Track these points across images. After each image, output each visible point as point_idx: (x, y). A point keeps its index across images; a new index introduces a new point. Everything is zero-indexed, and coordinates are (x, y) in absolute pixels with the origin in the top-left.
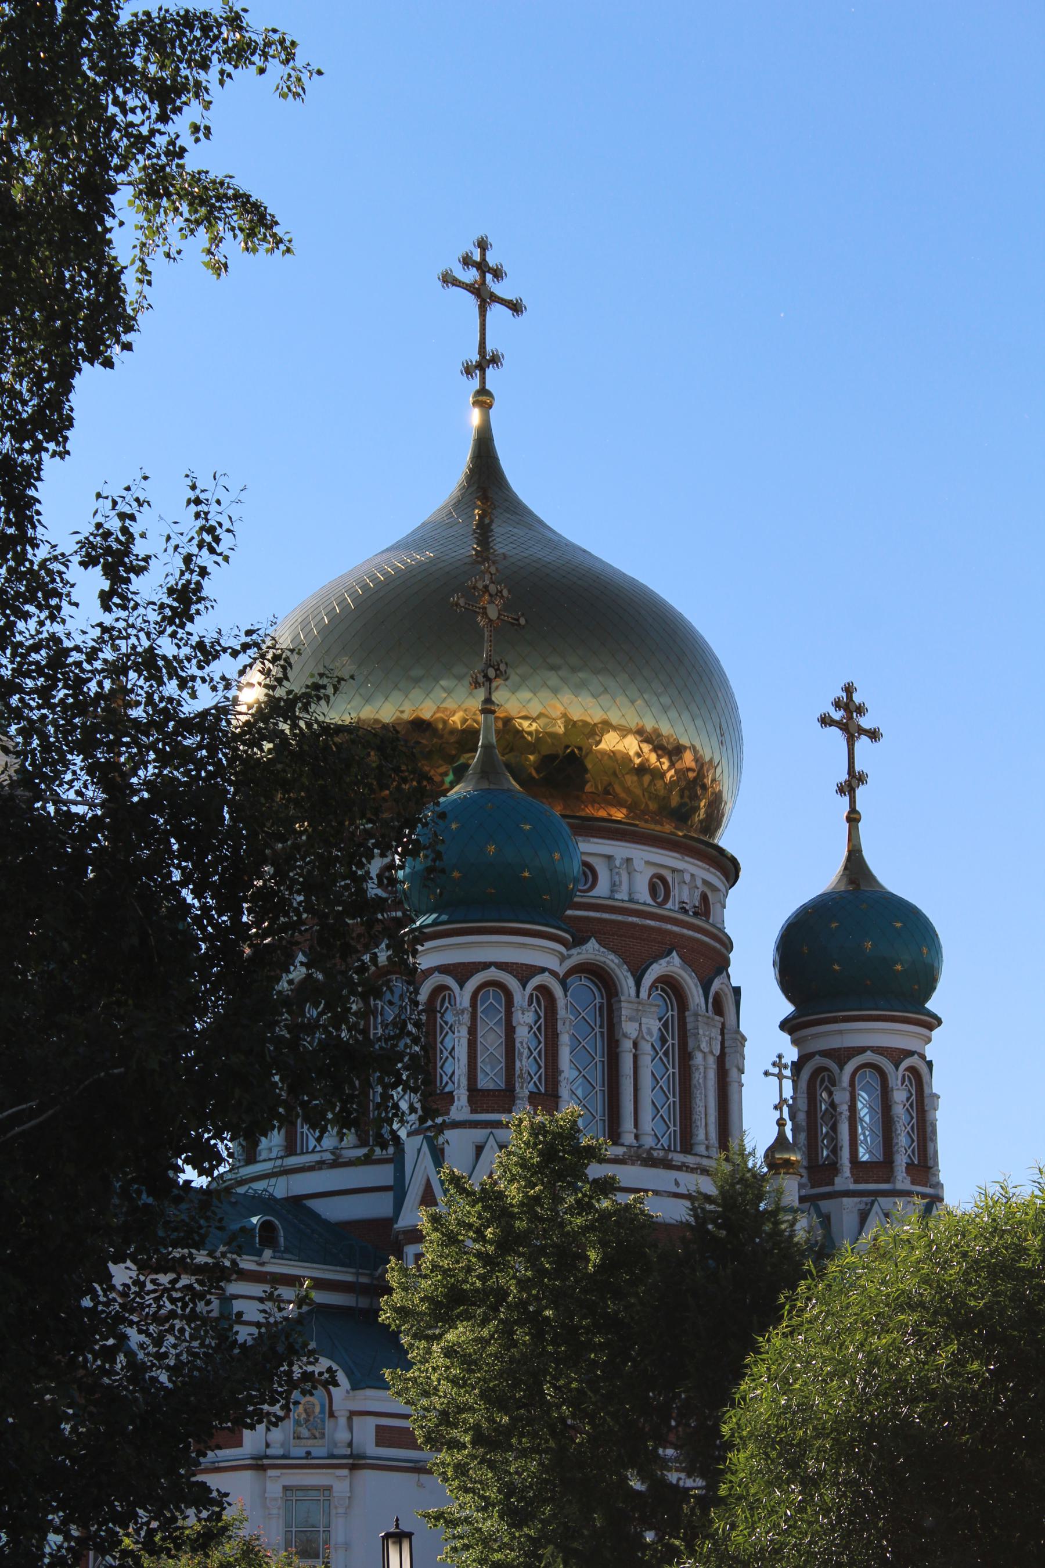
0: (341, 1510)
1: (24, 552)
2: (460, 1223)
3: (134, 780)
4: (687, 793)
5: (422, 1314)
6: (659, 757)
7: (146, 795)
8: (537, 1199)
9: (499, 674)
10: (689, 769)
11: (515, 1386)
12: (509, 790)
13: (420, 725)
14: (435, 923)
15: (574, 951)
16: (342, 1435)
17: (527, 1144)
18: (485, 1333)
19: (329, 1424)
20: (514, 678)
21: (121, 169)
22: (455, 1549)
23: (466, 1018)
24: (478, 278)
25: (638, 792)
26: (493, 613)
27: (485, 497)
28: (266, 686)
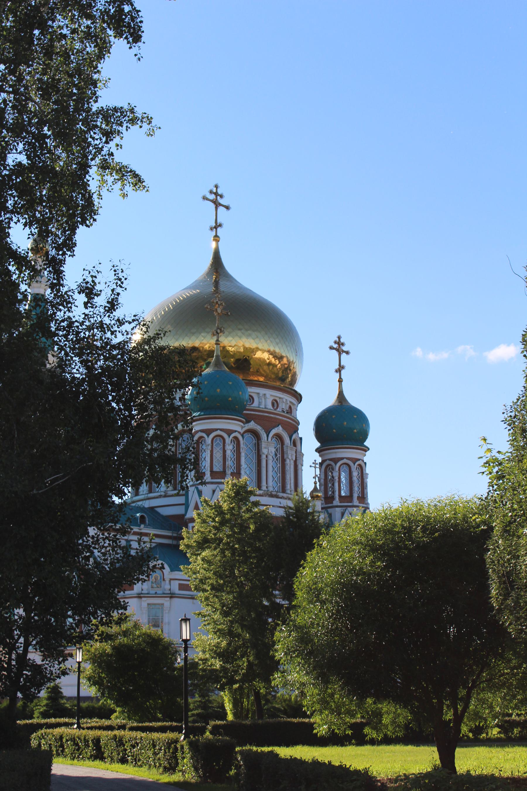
0: (167, 611)
1: (60, 289)
2: (207, 516)
3: (96, 366)
4: (284, 372)
5: (194, 546)
6: (275, 360)
7: (100, 371)
8: (233, 508)
9: (221, 331)
10: (285, 364)
11: (225, 570)
12: (224, 371)
13: (194, 349)
14: (199, 415)
15: (246, 425)
16: (167, 587)
17: (230, 489)
18: (215, 553)
19: (163, 583)
20: (226, 333)
21: (92, 159)
22: (205, 625)
23: (210, 447)
24: (215, 198)
25: (268, 371)
26: (219, 311)
27: (217, 272)
28: (141, 334)
